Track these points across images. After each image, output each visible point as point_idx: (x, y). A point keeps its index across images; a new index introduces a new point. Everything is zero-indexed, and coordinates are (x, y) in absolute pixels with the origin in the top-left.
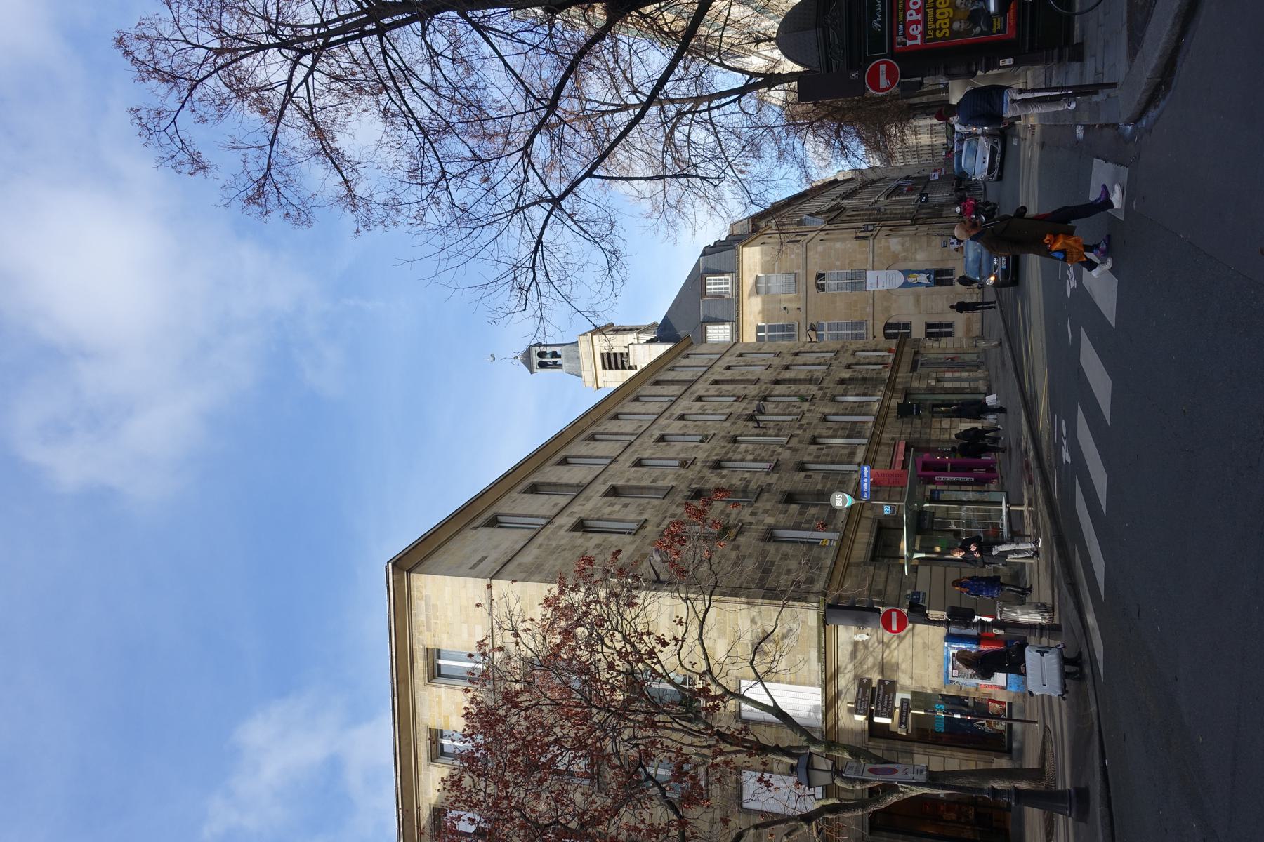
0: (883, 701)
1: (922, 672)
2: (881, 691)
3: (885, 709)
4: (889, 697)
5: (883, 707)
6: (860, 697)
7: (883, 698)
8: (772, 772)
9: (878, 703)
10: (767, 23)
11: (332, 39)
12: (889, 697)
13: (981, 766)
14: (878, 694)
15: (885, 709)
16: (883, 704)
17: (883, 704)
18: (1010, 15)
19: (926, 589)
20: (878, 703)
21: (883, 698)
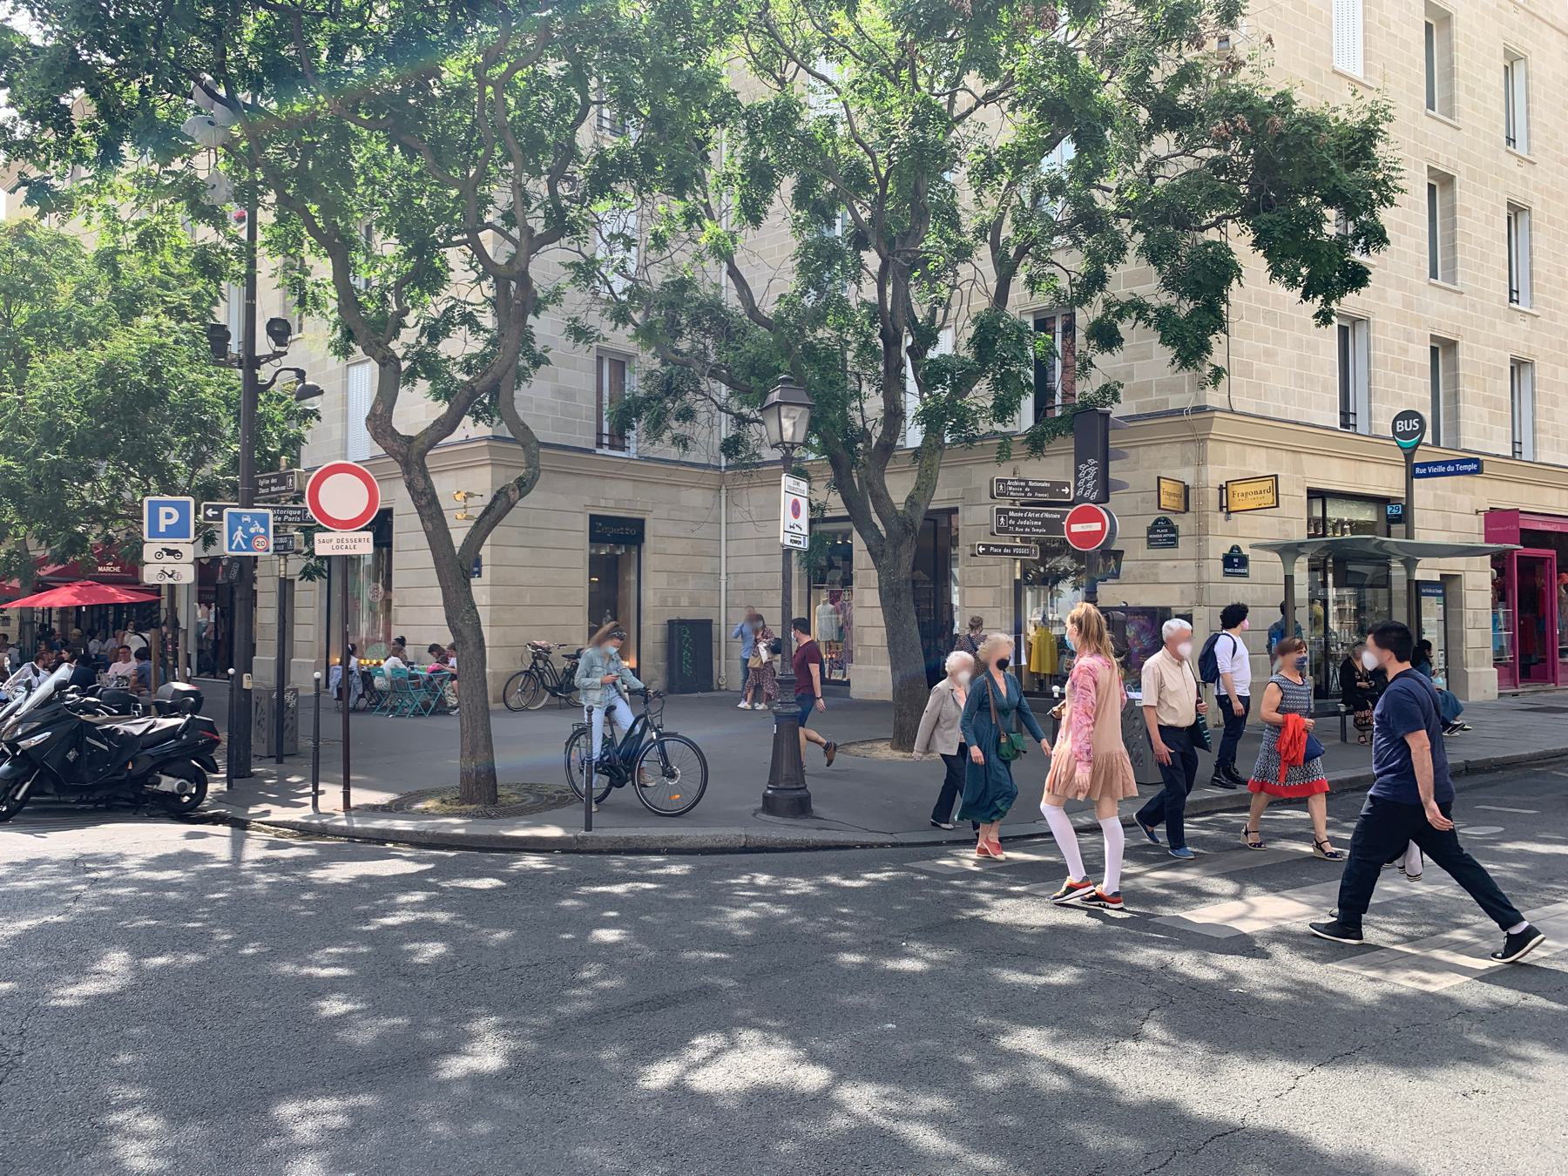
0: (1028, 519)
1: (633, 450)
2: (1047, 515)
3: (1011, 522)
4: (1036, 527)
5: (1016, 519)
6: (1030, 484)
7: (1034, 519)
8: (292, 208)
9: (1023, 511)
10: (136, 1030)
11: (455, 239)
12: (1036, 527)
13: (18, 713)
14: (1040, 512)
15: (1011, 522)
16: (1023, 519)
17: (1023, 519)
18: (1493, 870)
19: (1439, 573)
20: (1023, 511)
21: (1034, 519)
